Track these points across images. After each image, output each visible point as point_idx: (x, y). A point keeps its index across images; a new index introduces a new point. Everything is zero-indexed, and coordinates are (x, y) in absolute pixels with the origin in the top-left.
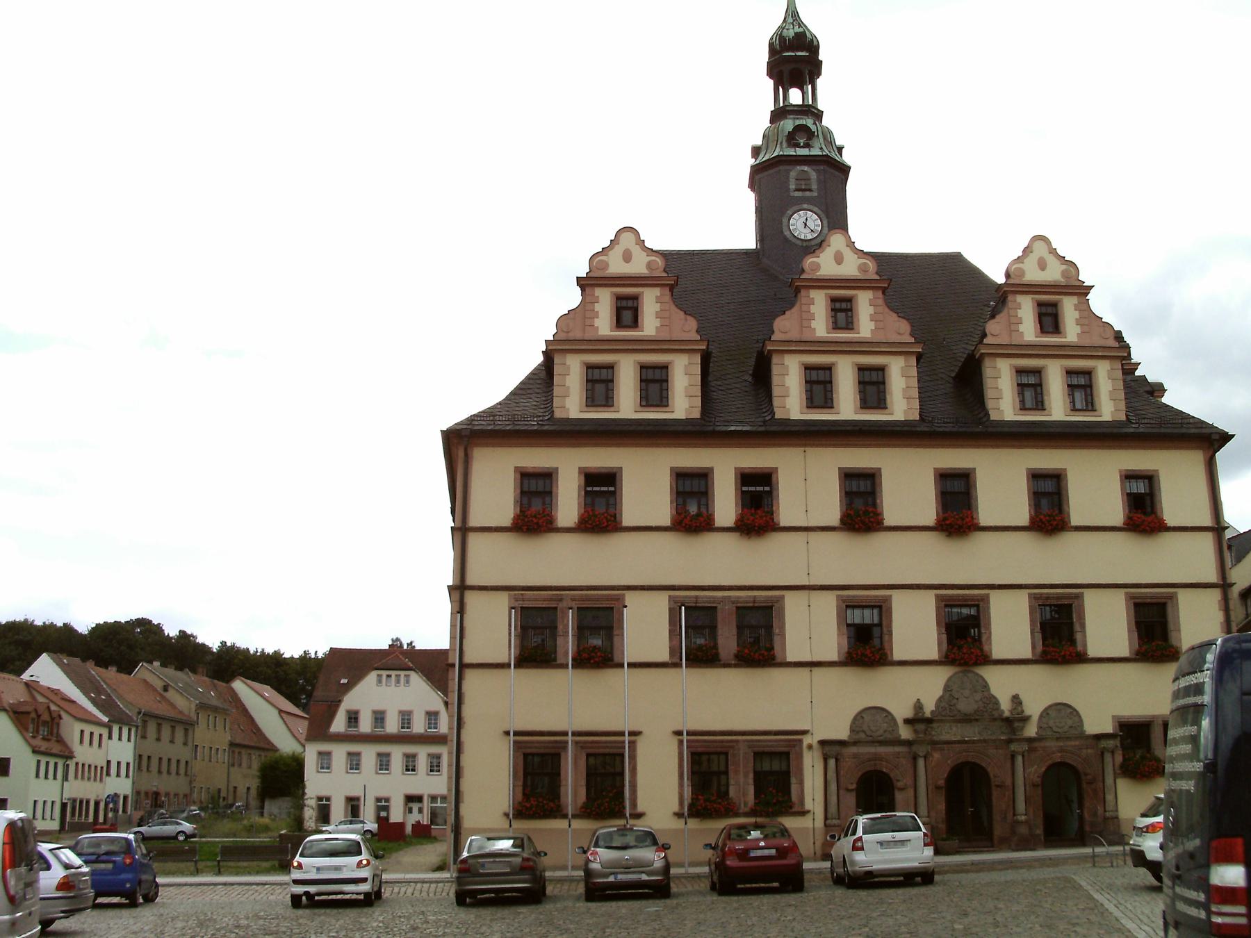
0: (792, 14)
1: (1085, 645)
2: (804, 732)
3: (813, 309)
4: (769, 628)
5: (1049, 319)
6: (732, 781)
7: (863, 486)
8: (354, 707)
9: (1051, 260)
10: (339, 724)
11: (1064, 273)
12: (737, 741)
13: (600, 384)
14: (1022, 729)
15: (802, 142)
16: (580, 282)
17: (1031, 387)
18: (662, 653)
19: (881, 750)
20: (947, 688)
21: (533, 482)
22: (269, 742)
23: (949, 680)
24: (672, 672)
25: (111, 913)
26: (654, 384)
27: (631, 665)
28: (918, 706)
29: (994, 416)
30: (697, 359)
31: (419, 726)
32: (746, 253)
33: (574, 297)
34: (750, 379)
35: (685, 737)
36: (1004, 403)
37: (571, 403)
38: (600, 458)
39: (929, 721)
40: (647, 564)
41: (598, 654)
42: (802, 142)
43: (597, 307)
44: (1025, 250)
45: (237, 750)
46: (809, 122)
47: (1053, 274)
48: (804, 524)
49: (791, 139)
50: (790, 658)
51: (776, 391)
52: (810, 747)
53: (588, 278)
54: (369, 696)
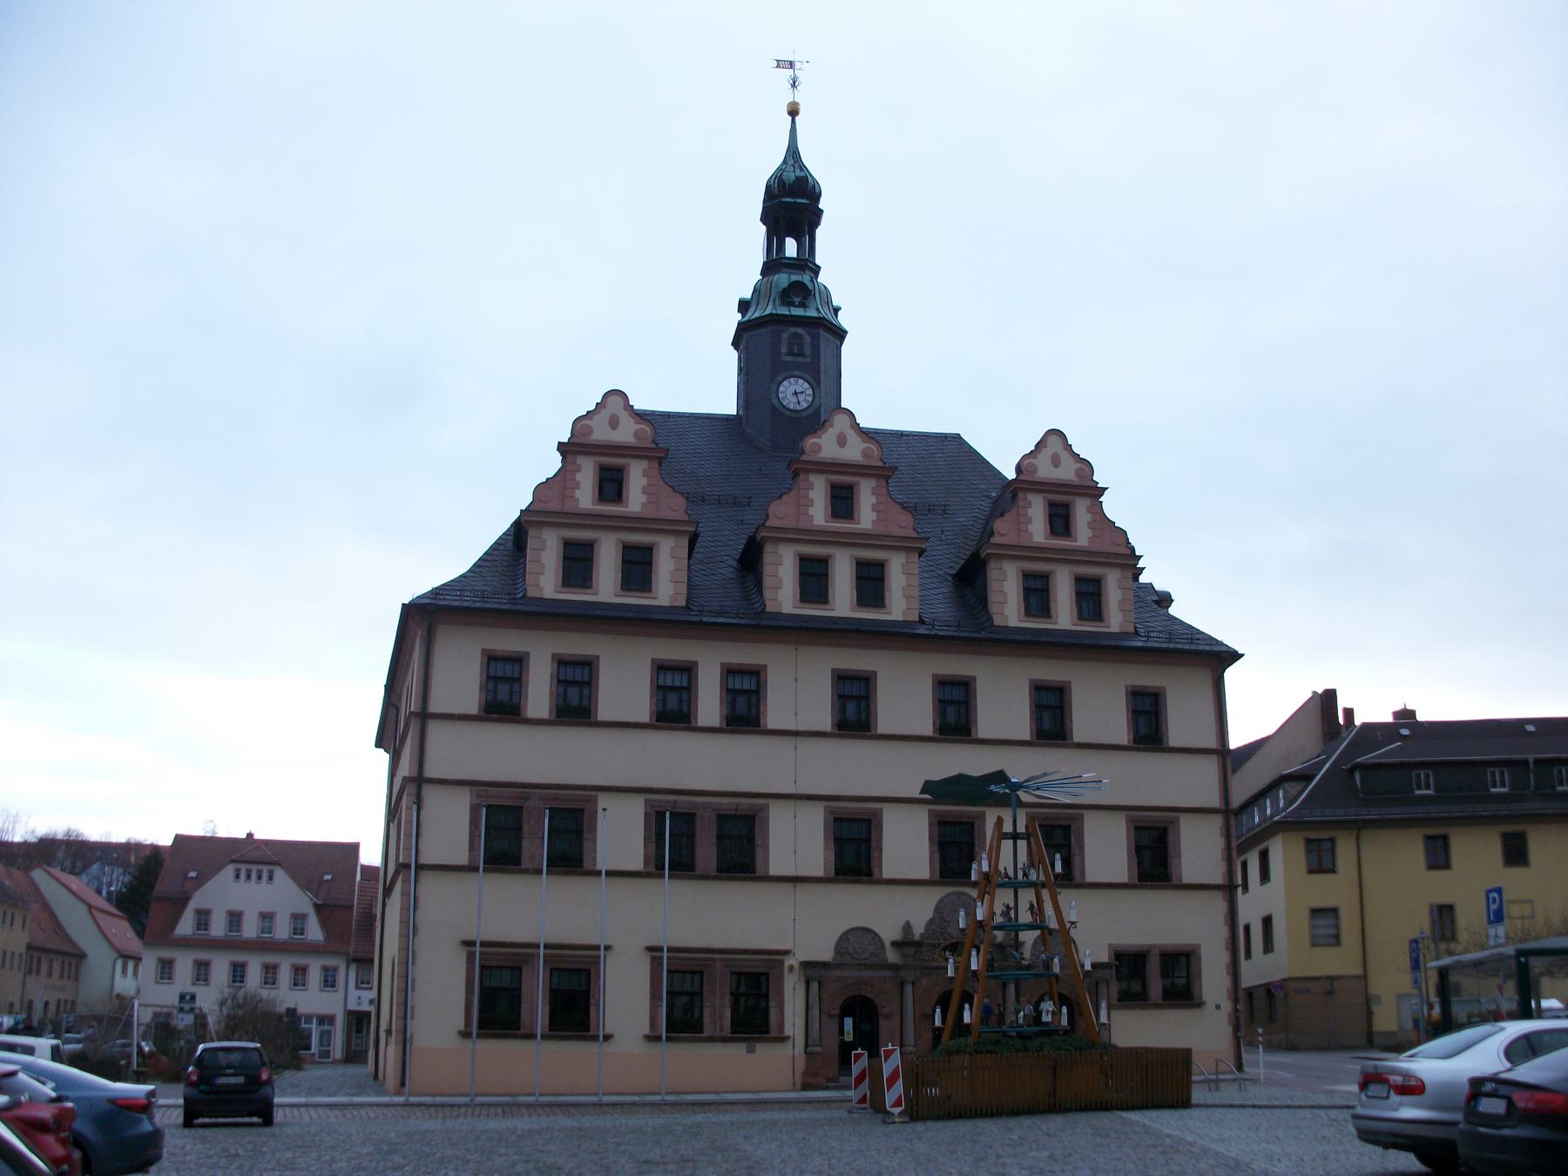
0: (793, 153)
1: (595, 859)
2: (786, 952)
3: (1030, 512)
4: (751, 839)
5: (1060, 520)
6: (706, 1003)
7: (678, 680)
8: (205, 905)
9: (1064, 455)
10: (186, 926)
11: (1077, 473)
12: (714, 960)
13: (578, 564)
14: (1070, 960)
15: (797, 300)
16: (562, 447)
17: (1037, 594)
18: (1122, 876)
19: (868, 974)
20: (937, 910)
21: (500, 666)
22: (74, 945)
23: (941, 901)
24: (469, 877)
25: (253, 1130)
26: (637, 568)
27: (610, 874)
28: (907, 927)
29: (997, 621)
30: (685, 542)
31: (282, 931)
32: (726, 419)
33: (554, 463)
34: (734, 564)
35: (478, 949)
36: (1008, 608)
37: (545, 580)
38: (577, 645)
39: (918, 944)
40: (624, 761)
41: (570, 856)
42: (797, 300)
43: (579, 477)
44: (1037, 446)
45: (36, 955)
46: (805, 278)
47: (1066, 473)
48: (793, 728)
49: (786, 296)
50: (1089, 878)
51: (768, 582)
52: (791, 968)
53: (569, 443)
54: (223, 894)
